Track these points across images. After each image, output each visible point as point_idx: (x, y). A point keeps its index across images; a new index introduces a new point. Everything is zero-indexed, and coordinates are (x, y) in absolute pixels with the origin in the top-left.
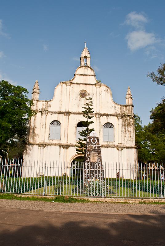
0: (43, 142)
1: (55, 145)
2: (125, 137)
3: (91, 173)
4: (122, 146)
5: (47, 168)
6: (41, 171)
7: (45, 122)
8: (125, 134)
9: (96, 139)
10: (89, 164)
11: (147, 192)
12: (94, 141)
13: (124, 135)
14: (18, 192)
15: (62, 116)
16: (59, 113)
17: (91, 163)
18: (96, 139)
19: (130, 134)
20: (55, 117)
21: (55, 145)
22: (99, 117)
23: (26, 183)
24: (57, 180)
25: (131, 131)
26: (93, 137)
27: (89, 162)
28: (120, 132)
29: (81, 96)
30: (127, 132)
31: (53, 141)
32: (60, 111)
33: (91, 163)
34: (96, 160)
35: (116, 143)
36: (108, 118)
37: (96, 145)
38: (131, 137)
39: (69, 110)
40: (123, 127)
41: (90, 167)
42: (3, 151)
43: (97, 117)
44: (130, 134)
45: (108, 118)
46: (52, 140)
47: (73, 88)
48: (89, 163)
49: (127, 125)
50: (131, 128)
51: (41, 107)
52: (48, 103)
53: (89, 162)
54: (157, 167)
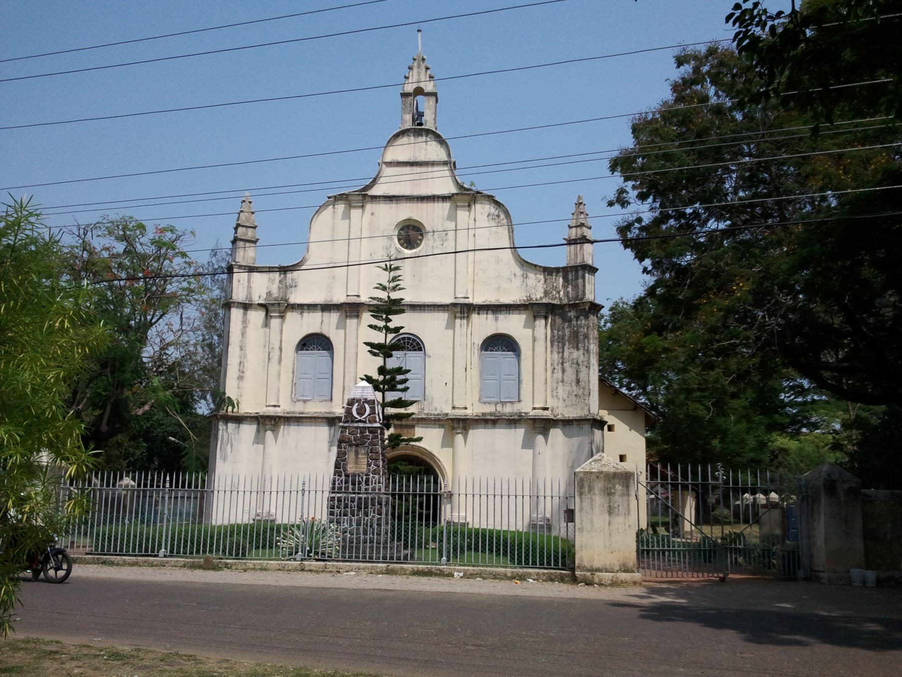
0: (272, 409)
1: (313, 420)
2: (560, 384)
3: (346, 506)
4: (547, 414)
5: (307, 493)
6: (266, 509)
7: (279, 340)
8: (560, 374)
9: (367, 406)
10: (342, 481)
11: (492, 552)
12: (361, 411)
13: (555, 375)
14: (116, 551)
15: (334, 317)
16: (326, 308)
17: (347, 476)
18: (367, 406)
19: (578, 372)
20: (312, 323)
21: (313, 420)
22: (466, 315)
23: (186, 536)
24: (448, 545)
25: (580, 361)
26: (358, 401)
27: (343, 474)
28: (540, 369)
29: (402, 241)
30: (566, 365)
31: (308, 404)
32: (329, 299)
33: (347, 476)
34: (364, 468)
35: (526, 407)
36: (496, 319)
37: (365, 422)
38: (578, 381)
39: (358, 296)
40: (552, 346)
41: (347, 488)
42: (171, 438)
43: (458, 315)
44: (578, 372)
45: (496, 319)
46: (305, 401)
47: (372, 214)
48: (343, 477)
49: (567, 338)
50: (581, 351)
51: (266, 291)
52: (289, 275)
53: (343, 474)
54: (135, 481)
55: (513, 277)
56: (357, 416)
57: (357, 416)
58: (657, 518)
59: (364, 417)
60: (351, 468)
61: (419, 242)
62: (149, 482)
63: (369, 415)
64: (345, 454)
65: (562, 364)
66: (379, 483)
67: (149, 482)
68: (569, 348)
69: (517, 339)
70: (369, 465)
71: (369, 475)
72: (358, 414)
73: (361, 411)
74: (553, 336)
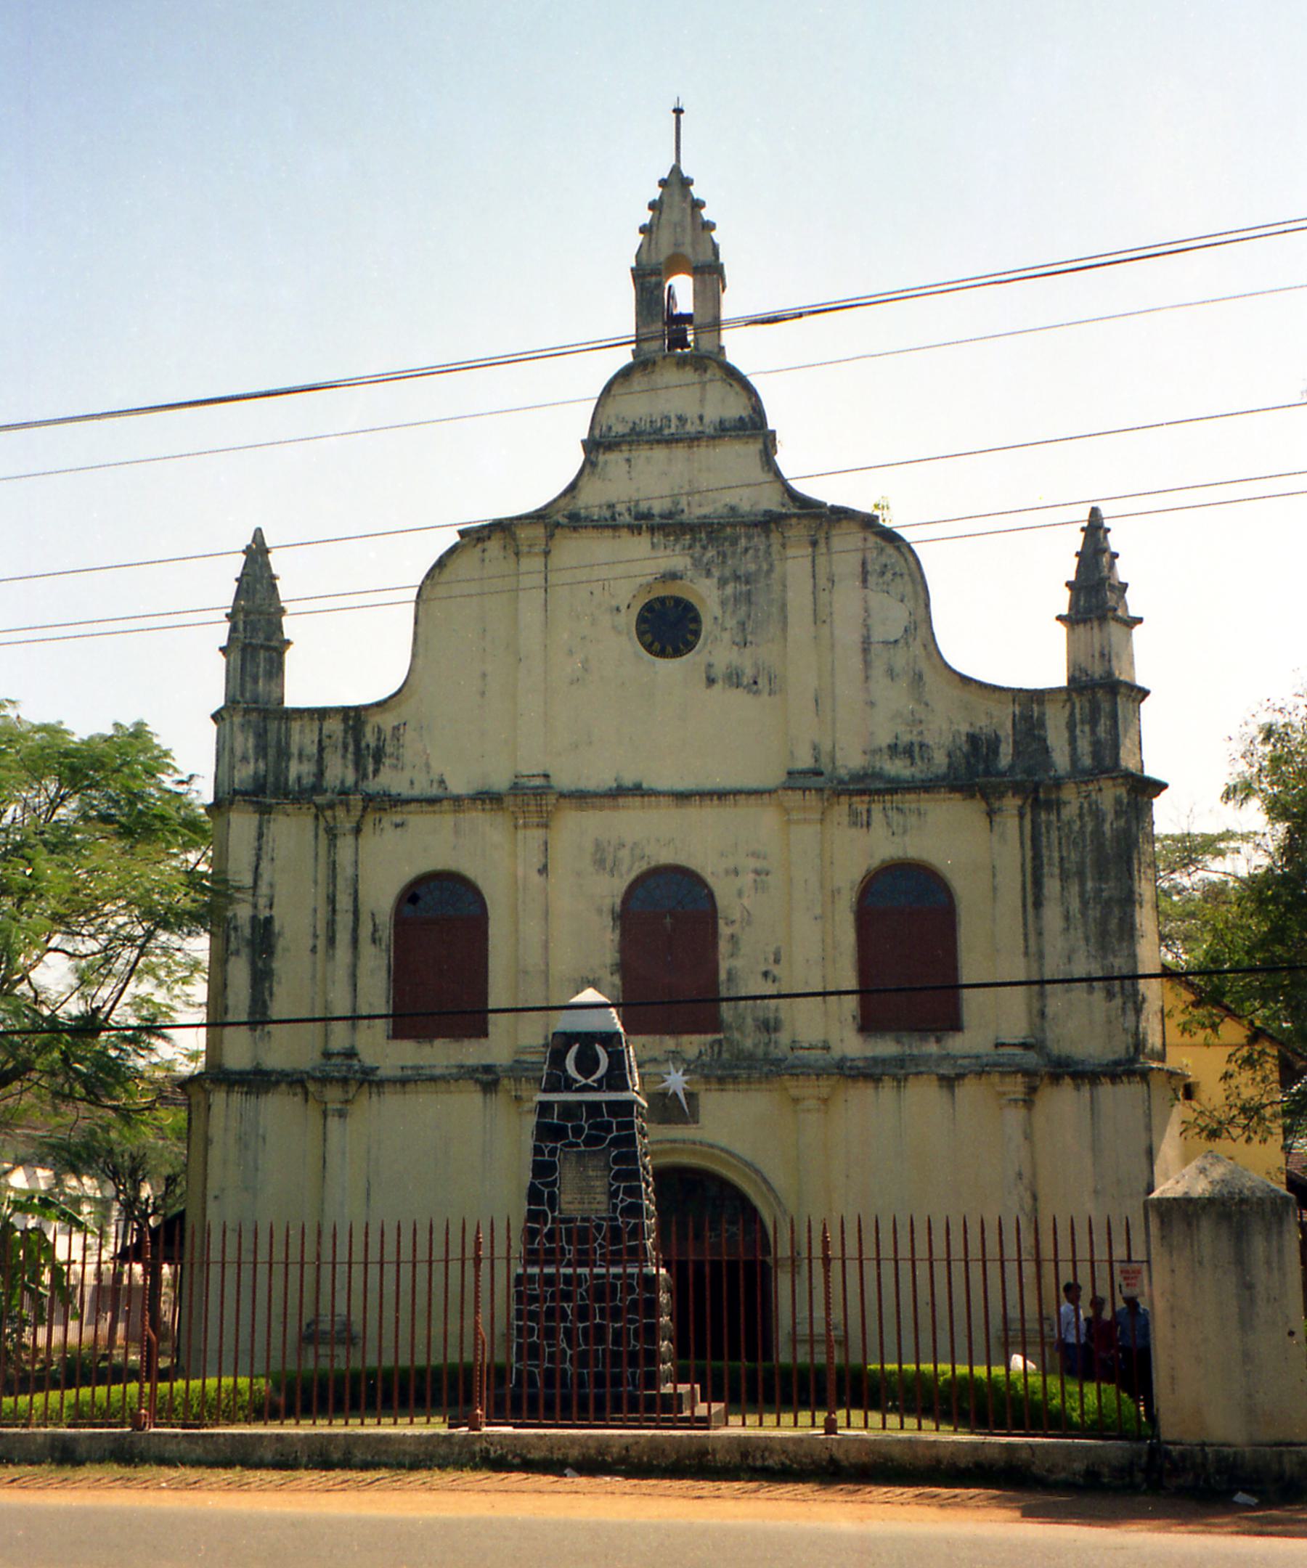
18: (600, 1050)
56: (579, 1077)
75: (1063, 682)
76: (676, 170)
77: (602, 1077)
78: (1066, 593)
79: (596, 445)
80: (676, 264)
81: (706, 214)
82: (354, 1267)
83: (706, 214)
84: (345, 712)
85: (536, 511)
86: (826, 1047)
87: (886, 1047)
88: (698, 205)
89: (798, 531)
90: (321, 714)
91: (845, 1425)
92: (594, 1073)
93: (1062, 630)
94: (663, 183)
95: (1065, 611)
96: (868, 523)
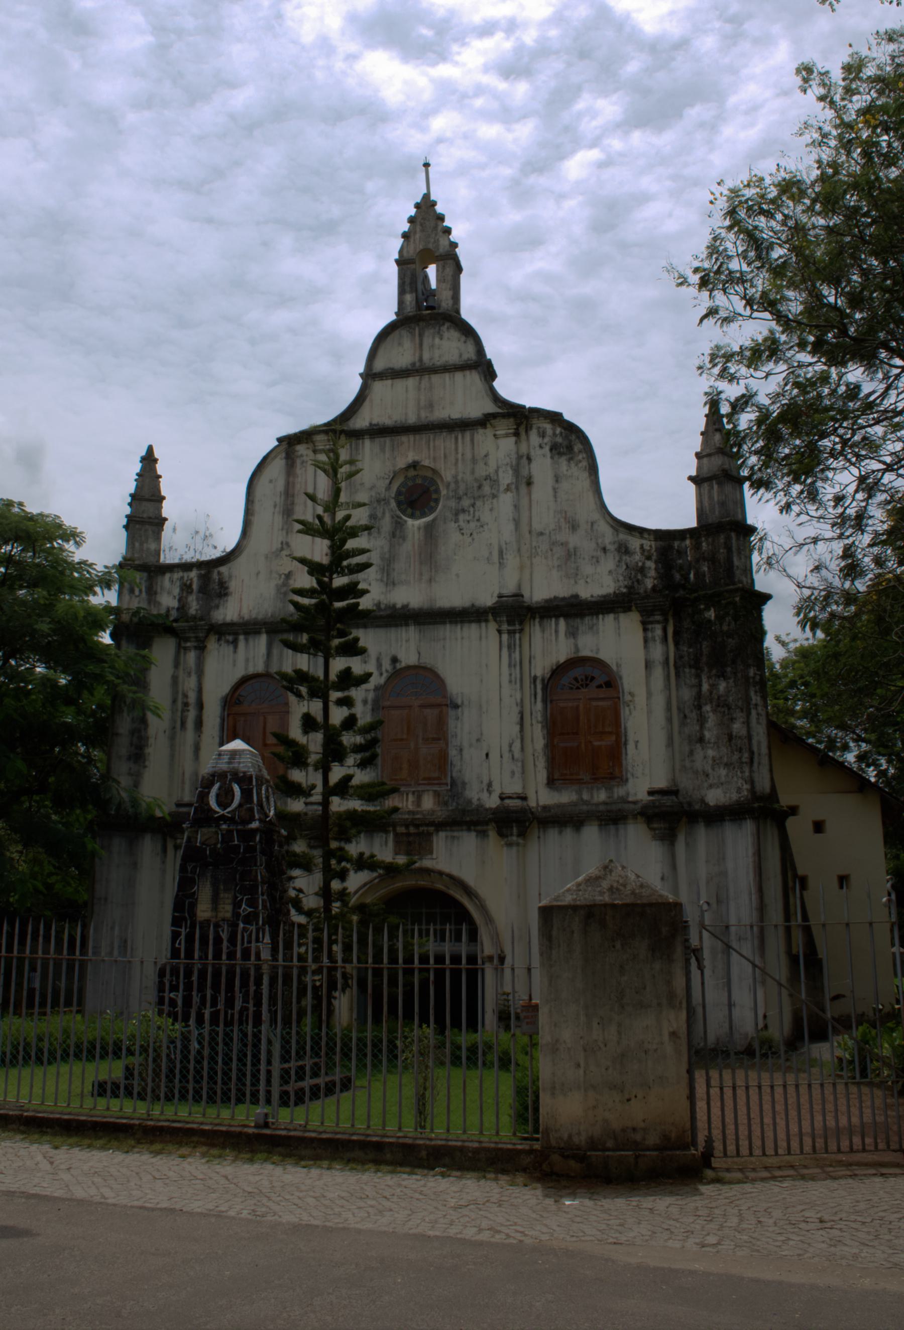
12: (225, 798)
18: (236, 788)
34: (226, 910)
55: (600, 553)
56: (217, 809)
57: (217, 809)
58: (475, 1035)
59: (229, 809)
60: (203, 911)
61: (432, 504)
62: (41, 932)
63: (240, 805)
64: (192, 882)
65: (699, 707)
66: (257, 941)
67: (41, 932)
68: (709, 678)
69: (348, 658)
70: (237, 905)
71: (237, 925)
72: (219, 804)
73: (225, 798)
74: (679, 657)
75: (693, 523)
76: (427, 196)
77: (236, 808)
78: (159, 472)
79: (370, 376)
80: (427, 256)
81: (447, 223)
82: (751, 1092)
83: (447, 223)
84: (200, 565)
85: (326, 425)
86: (524, 798)
87: (565, 797)
88: (441, 218)
89: (504, 427)
90: (186, 567)
91: (773, 1153)
92: (230, 805)
93: (692, 487)
94: (417, 206)
95: (694, 473)
96: (555, 418)
